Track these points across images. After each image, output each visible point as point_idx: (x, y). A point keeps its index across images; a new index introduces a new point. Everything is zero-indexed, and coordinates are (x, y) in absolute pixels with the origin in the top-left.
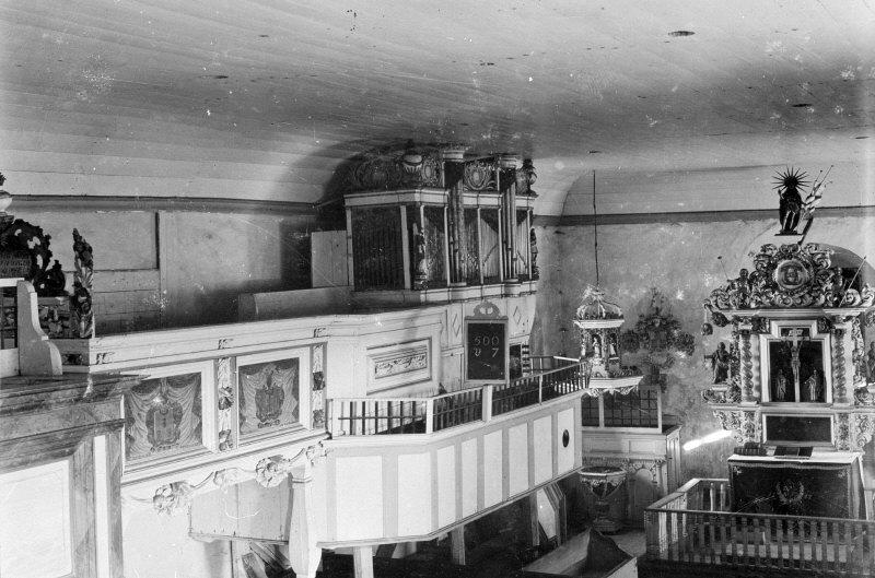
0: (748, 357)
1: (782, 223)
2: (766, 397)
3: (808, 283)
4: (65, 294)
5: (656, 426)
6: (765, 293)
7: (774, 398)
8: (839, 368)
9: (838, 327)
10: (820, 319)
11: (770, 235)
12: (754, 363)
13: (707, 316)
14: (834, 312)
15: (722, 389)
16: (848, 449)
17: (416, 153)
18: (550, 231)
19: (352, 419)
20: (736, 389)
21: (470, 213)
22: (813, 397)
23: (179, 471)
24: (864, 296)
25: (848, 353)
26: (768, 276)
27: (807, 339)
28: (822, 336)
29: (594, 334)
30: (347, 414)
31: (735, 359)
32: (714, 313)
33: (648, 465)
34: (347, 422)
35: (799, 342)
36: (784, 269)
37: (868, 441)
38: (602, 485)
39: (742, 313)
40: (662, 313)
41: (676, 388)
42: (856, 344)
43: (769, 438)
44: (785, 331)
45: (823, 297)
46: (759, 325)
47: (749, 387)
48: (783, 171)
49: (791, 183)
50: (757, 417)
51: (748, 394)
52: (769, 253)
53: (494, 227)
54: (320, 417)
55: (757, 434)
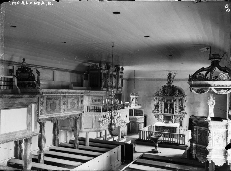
4: (35, 81)
11: (165, 83)
18: (126, 81)
19: (88, 109)
21: (112, 75)
23: (142, 137)
30: (87, 108)
34: (87, 110)
48: (169, 72)
49: (170, 74)
53: (115, 78)
54: (78, 107)
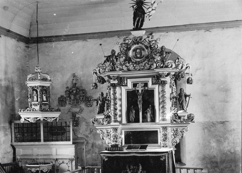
0: (115, 99)
1: (134, 26)
2: (124, 121)
3: (147, 57)
5: (69, 140)
6: (124, 64)
7: (129, 121)
8: (162, 102)
9: (162, 79)
10: (153, 77)
12: (119, 103)
13: (94, 78)
14: (160, 71)
15: (101, 117)
16: (167, 146)
17: (42, 88)
20: (108, 117)
22: (149, 119)
24: (177, 64)
25: (168, 95)
26: (126, 54)
27: (146, 88)
28: (154, 86)
29: (34, 89)
31: (108, 101)
32: (98, 77)
33: (66, 161)
35: (142, 90)
36: (135, 50)
37: (178, 143)
38: (38, 171)
39: (112, 74)
40: (77, 85)
41: (84, 123)
42: (172, 89)
43: (125, 143)
44: (135, 85)
45: (155, 65)
46: (121, 81)
47: (116, 115)
50: (119, 131)
51: (115, 118)
52: (127, 42)
55: (119, 140)
